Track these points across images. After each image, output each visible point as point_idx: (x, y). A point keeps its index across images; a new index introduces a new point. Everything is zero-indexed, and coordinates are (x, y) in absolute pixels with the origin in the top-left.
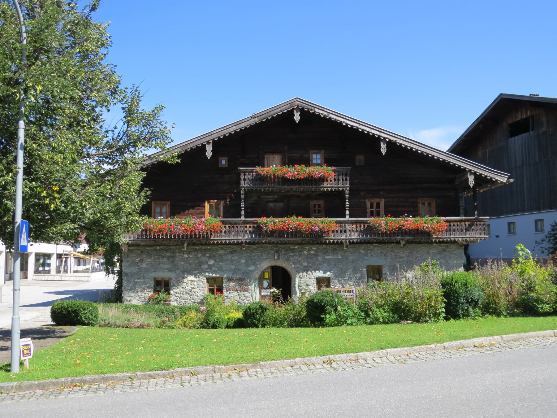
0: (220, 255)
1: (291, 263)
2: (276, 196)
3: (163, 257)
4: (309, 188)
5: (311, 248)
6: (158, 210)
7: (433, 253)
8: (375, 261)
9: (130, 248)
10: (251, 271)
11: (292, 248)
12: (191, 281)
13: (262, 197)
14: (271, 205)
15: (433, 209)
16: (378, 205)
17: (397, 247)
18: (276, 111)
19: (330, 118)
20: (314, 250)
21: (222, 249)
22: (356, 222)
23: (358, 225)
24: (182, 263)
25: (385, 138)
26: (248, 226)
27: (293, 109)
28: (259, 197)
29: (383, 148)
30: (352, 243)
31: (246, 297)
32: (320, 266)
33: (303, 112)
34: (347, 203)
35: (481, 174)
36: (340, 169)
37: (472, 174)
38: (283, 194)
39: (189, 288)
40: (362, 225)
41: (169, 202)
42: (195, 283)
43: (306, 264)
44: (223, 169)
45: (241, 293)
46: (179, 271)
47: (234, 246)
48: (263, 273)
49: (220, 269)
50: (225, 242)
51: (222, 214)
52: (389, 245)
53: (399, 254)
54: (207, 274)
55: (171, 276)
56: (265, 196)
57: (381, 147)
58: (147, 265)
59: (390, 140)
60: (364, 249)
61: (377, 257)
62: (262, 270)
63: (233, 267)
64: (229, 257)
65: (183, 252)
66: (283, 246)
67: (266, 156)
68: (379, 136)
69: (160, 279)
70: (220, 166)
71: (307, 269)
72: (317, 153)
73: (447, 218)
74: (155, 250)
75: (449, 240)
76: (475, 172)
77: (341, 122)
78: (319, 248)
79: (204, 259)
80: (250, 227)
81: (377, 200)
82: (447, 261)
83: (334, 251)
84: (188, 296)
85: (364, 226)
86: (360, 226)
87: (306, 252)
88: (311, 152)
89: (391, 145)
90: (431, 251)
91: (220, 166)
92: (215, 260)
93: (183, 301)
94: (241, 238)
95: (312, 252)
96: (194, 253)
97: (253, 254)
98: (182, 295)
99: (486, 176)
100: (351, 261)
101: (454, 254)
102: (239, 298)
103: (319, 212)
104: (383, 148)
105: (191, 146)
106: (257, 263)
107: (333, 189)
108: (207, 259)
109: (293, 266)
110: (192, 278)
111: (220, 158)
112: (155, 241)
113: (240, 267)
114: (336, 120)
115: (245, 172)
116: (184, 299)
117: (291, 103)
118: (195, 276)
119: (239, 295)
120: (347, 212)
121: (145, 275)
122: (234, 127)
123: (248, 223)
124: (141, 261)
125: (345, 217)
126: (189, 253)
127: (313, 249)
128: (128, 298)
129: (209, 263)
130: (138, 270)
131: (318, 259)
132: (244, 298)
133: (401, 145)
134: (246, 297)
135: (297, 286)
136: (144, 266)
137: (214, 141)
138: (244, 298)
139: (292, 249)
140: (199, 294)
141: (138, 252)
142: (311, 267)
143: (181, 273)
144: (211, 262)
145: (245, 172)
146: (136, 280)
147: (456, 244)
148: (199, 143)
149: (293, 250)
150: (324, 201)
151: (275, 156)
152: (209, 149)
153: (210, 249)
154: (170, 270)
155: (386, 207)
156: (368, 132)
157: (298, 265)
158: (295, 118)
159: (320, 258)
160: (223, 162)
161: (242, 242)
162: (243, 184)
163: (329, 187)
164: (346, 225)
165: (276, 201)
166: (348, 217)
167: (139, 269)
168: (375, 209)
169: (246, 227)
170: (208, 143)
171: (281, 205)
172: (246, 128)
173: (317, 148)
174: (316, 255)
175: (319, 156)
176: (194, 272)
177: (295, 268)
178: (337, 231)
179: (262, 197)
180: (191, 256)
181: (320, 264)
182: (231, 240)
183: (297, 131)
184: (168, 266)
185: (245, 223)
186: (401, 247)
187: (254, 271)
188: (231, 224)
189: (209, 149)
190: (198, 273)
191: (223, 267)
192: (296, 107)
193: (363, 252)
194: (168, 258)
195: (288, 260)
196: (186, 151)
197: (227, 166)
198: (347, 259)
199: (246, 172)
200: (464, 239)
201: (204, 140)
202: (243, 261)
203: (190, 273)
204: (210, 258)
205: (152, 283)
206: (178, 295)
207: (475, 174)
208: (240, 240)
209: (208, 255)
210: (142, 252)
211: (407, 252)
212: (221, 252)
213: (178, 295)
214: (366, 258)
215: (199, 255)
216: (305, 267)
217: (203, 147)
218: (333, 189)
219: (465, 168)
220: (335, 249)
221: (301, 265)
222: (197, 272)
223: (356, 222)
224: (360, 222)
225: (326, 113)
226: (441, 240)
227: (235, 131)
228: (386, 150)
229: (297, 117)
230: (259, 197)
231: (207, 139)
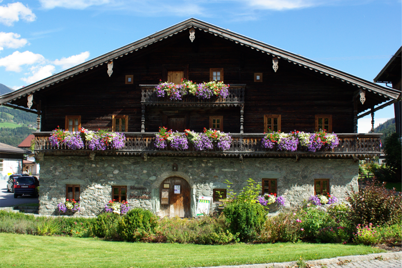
0: (124, 166)
1: (189, 174)
2: (177, 112)
3: (74, 166)
4: (198, 104)
5: (209, 161)
6: (71, 123)
7: (328, 168)
8: (270, 174)
9: (45, 157)
10: (153, 181)
11: (191, 160)
12: (98, 189)
13: (164, 112)
14: (174, 120)
15: (330, 126)
16: (275, 122)
17: (293, 161)
19: (224, 37)
20: (211, 163)
21: (126, 160)
22: (250, 137)
23: (252, 140)
24: (90, 172)
25: (276, 56)
26: (147, 139)
27: (189, 29)
29: (275, 65)
30: (246, 157)
31: (147, 205)
32: (217, 178)
33: (199, 33)
34: (242, 119)
35: (372, 91)
36: (234, 86)
37: (363, 91)
39: (96, 195)
40: (256, 140)
41: (80, 117)
42: (102, 191)
43: (203, 176)
45: (143, 201)
46: (87, 179)
47: (137, 158)
48: (163, 183)
49: (124, 178)
50: (126, 154)
51: (127, 128)
52: (284, 159)
53: (293, 168)
54: (112, 183)
55: (81, 184)
56: (167, 112)
57: (273, 64)
58: (60, 172)
59: (282, 58)
60: (259, 163)
61: (272, 170)
62: (162, 181)
63: (136, 177)
64: (132, 167)
65: (92, 162)
66: (183, 159)
67: (169, 74)
68: (271, 54)
69: (71, 186)
71: (204, 181)
72: (217, 71)
73: (234, 134)
74: (67, 159)
75: (341, 155)
76: (367, 89)
77: (234, 41)
78: (216, 161)
79: (109, 169)
80: (149, 140)
81: (274, 116)
82: (341, 176)
83: (231, 164)
84: (95, 202)
85: (257, 141)
86: (254, 141)
87: (203, 165)
88: (211, 69)
89: (282, 62)
90: (326, 166)
92: (119, 170)
93: (90, 207)
94: (140, 150)
95: (210, 165)
96: (100, 163)
97: (154, 165)
98: (89, 201)
99: (378, 93)
100: (246, 174)
101: (349, 169)
102: (141, 205)
103: (218, 126)
104: (275, 65)
105: (98, 63)
106: (158, 173)
107: (229, 105)
108: (112, 168)
109: (191, 177)
110: (99, 186)
111: (126, 76)
112: (64, 152)
113: (142, 177)
115: (145, 89)
116: (91, 205)
117: (186, 23)
118: (102, 185)
119: (141, 203)
120: (242, 127)
121: (58, 182)
122: (133, 47)
123: (147, 137)
124: (55, 169)
125: (239, 132)
126: (96, 163)
127: (211, 161)
128: (44, 202)
129: (114, 173)
130: (52, 177)
131: (215, 172)
132: (145, 206)
134: (147, 205)
135: (194, 196)
136: (57, 173)
137: (114, 60)
138: (145, 206)
139: (191, 161)
140: (104, 201)
141: (52, 161)
142: (208, 179)
143: (89, 181)
144: (116, 172)
145: (145, 89)
146: (50, 186)
147: (352, 160)
148: (101, 62)
149: (191, 163)
150: (222, 117)
151: (177, 73)
152: (110, 67)
153: (115, 160)
154: (80, 178)
155: (282, 123)
156: (261, 51)
157: (195, 177)
158: (190, 38)
159: (217, 170)
160: (130, 80)
162: (143, 100)
163: (224, 103)
164: (240, 139)
165: (177, 116)
166: (242, 132)
167: (53, 176)
168: (272, 125)
169: (145, 140)
170: (109, 62)
171: (183, 120)
172: (144, 47)
173: (217, 67)
174: (213, 168)
175: (219, 74)
176: (101, 180)
177: (193, 179)
179: (164, 112)
180: (98, 166)
181: (217, 177)
182: (132, 152)
183: (194, 48)
184: (79, 175)
185: (144, 136)
186: (296, 162)
187: (155, 181)
188: (131, 137)
189: (110, 67)
190: (104, 182)
191: (127, 177)
192: (191, 27)
193: (258, 165)
194: (79, 167)
195: (187, 172)
197: (132, 83)
198: (243, 172)
199: (147, 89)
200: (357, 155)
201: (105, 60)
202: (145, 172)
203: (97, 182)
204: (115, 168)
205: (64, 190)
206: (86, 201)
208: (139, 152)
209: (113, 165)
211: (302, 166)
212: (125, 163)
213: (86, 201)
214: (262, 171)
215: (106, 165)
216: (203, 178)
217: (105, 66)
218: (229, 105)
219: (356, 85)
220: (231, 162)
221: (199, 176)
222: (104, 180)
223: (250, 137)
224: (253, 137)
225: (220, 33)
226: (333, 155)
227: (134, 51)
228: (277, 67)
229: (192, 36)
231: (108, 58)
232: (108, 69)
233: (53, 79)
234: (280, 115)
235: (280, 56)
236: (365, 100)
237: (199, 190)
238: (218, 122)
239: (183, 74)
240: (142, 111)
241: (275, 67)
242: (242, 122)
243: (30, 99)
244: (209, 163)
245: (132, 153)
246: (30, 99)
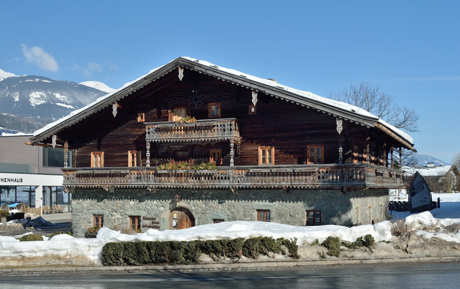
5: (208, 192)
13: (171, 146)
18: (163, 71)
28: (169, 147)
38: (188, 144)
44: (253, 115)
56: (173, 146)
68: (250, 88)
70: (250, 113)
77: (217, 77)
90: (317, 198)
91: (250, 113)
94: (145, 183)
114: (212, 75)
125: (63, 167)
133: (270, 95)
153: (131, 192)
161: (229, 187)
165: (182, 150)
178: (222, 178)
179: (171, 146)
183: (184, 88)
196: (98, 111)
201: (253, 86)
207: (343, 119)
208: (145, 185)
210: (84, 193)
217: (110, 107)
229: (181, 75)
230: (169, 147)
232: (252, 98)
233: (70, 121)
234: (103, 153)
235: (258, 89)
236: (342, 129)
237: (200, 221)
238: (218, 153)
239: (185, 110)
240: (231, 144)
241: (255, 101)
242: (341, 152)
243: (54, 139)
244: (209, 194)
245: (139, 186)
246: (54, 139)
